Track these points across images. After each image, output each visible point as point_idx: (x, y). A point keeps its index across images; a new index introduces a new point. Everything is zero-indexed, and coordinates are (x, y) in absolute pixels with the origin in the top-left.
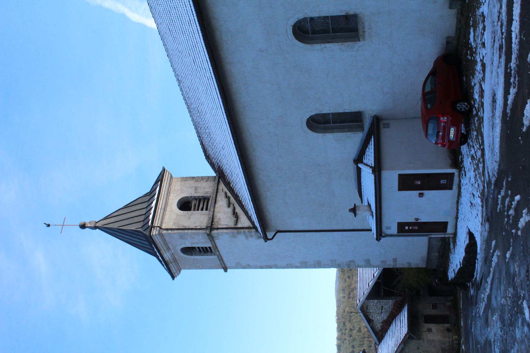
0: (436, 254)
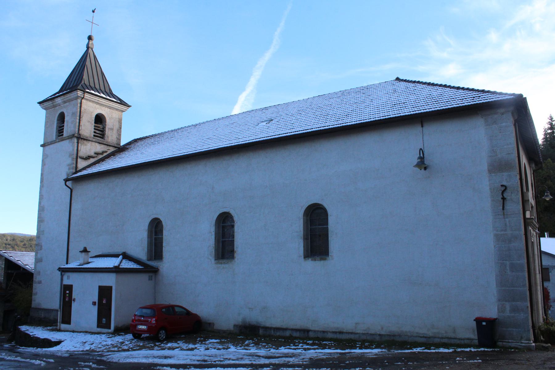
0: (43, 316)
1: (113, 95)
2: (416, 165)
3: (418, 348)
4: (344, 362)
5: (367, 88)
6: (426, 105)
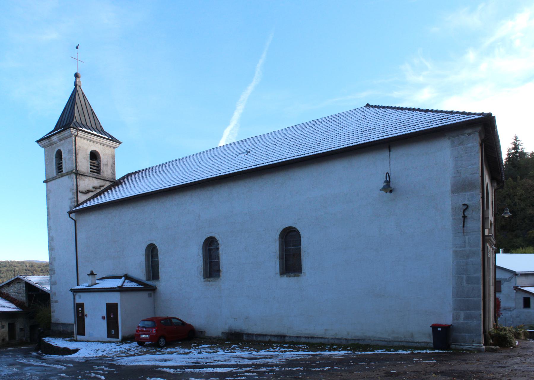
2: (382, 188)
3: (379, 350)
4: (315, 362)
5: (338, 116)
6: (395, 130)
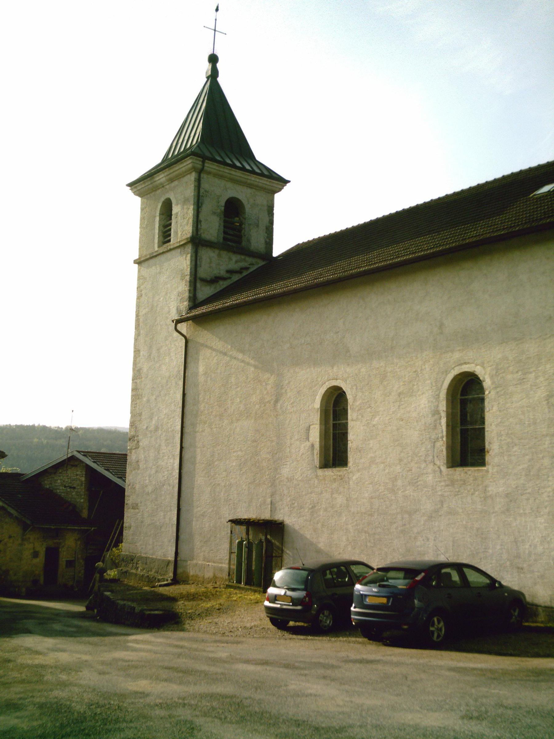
1: (256, 162)
